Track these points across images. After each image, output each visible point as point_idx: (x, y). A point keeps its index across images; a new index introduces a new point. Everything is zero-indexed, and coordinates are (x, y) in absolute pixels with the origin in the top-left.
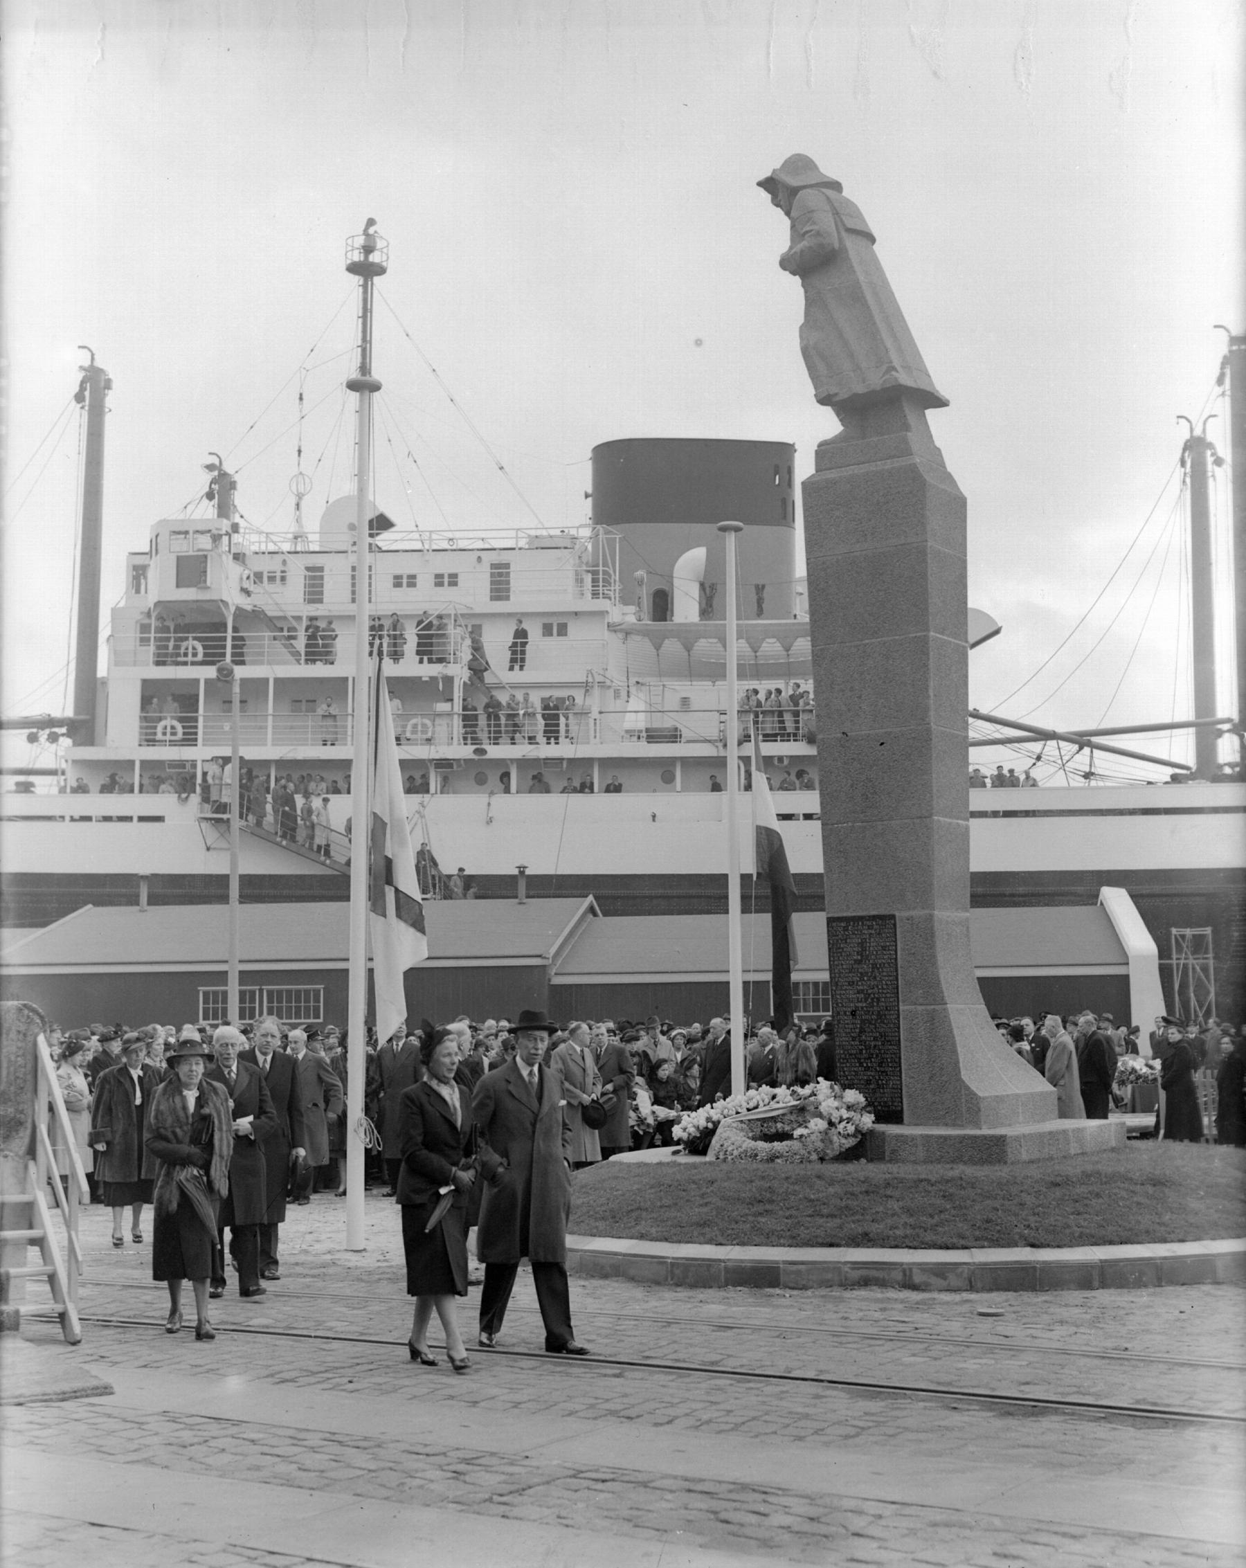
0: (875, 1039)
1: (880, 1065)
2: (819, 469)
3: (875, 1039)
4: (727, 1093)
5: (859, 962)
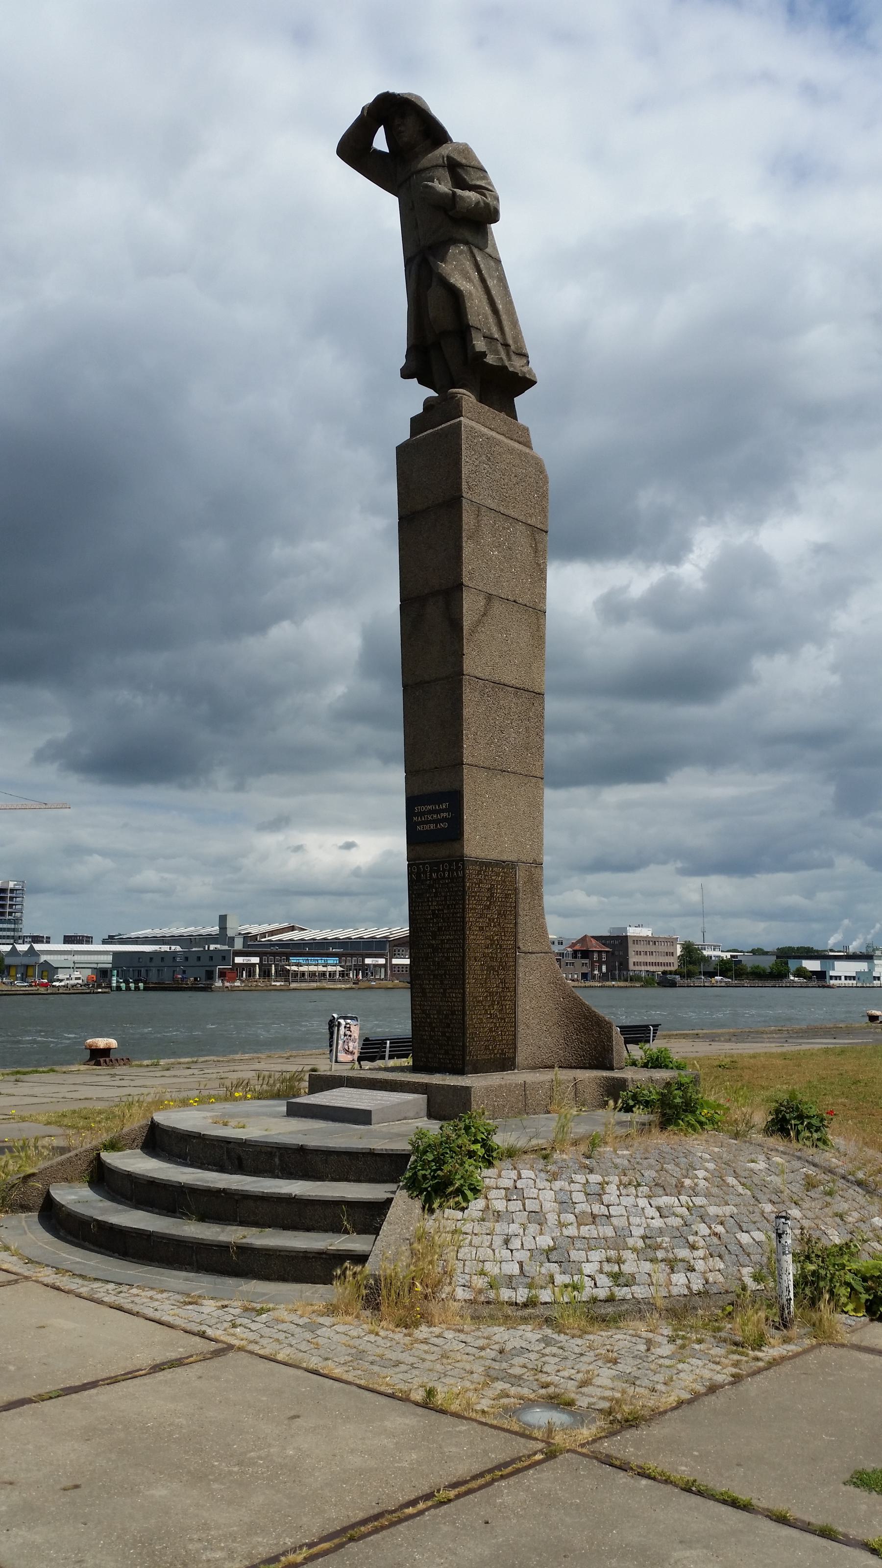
2: (413, 433)
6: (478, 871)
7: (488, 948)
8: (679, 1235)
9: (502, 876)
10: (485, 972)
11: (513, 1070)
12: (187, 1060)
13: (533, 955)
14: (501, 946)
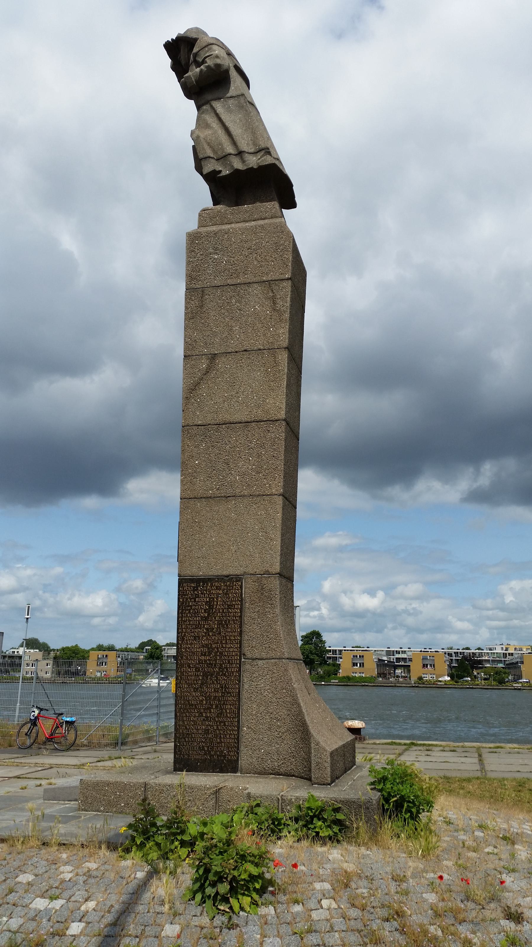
0: (216, 691)
1: (219, 715)
2: (201, 225)
3: (216, 691)
4: (213, 888)
5: (206, 619)
6: (194, 587)
7: (205, 655)
8: (20, 930)
10: (201, 678)
12: (492, 745)
14: (221, 653)
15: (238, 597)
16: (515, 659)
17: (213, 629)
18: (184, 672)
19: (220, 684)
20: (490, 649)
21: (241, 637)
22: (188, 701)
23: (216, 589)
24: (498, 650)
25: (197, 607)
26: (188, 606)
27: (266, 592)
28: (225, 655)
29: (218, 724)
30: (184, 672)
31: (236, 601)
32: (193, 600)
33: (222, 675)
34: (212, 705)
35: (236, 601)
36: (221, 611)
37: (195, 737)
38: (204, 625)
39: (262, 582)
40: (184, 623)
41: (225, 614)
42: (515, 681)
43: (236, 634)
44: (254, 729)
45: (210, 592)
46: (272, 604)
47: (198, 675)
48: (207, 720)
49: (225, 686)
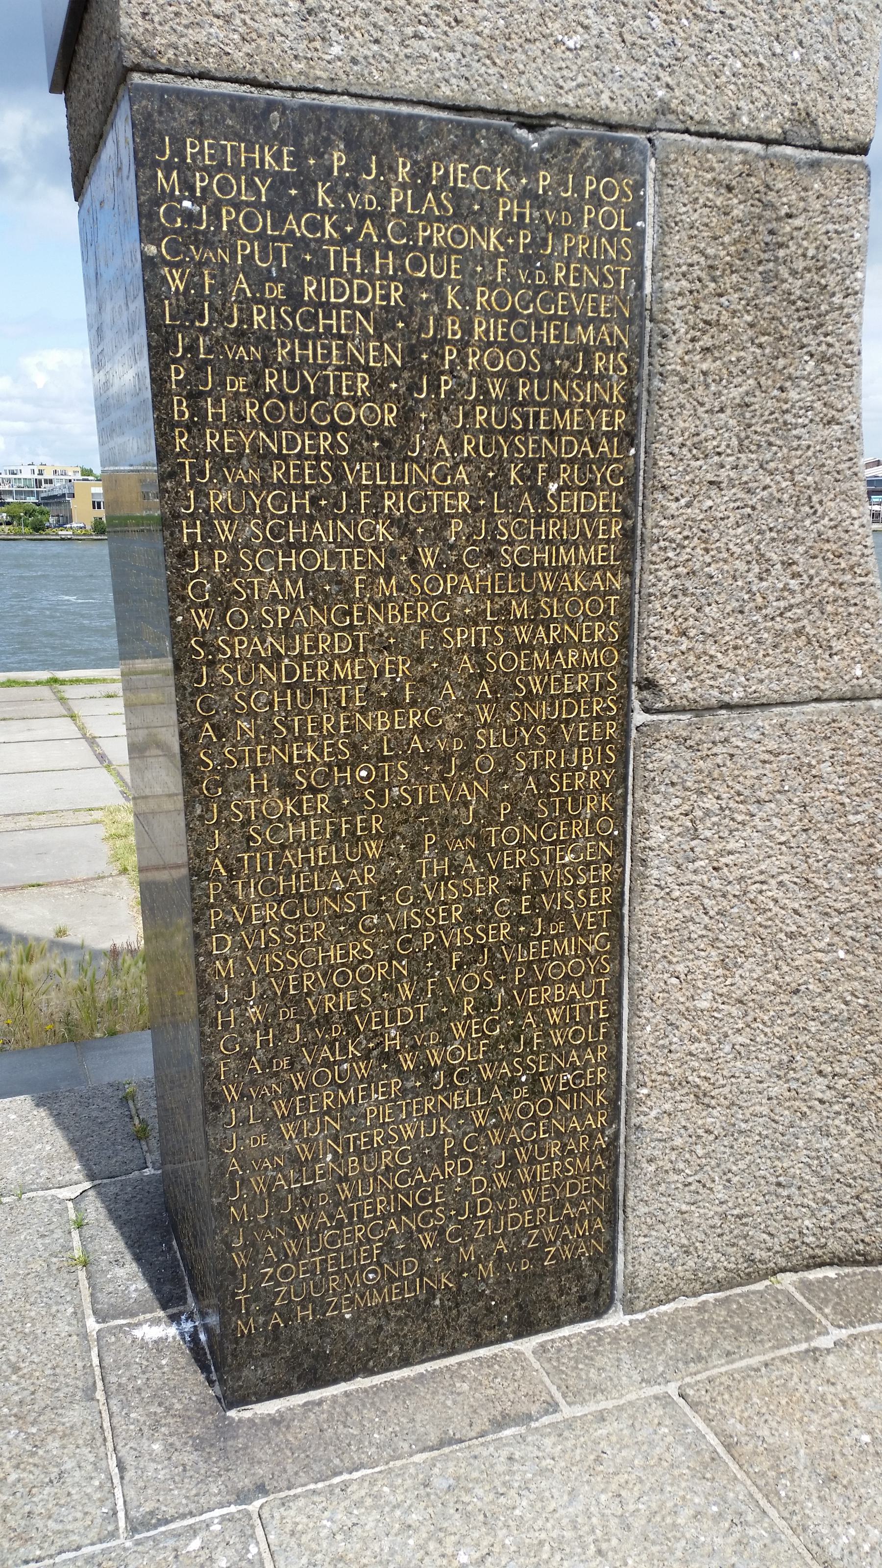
6: (280, 181)
7: (393, 703)
9: (512, 227)
10: (373, 850)
11: (598, 1314)
13: (759, 718)
15: (616, 290)
16: (58, 487)
17: (444, 521)
18: (247, 823)
19: (499, 871)
20: (13, 473)
21: (630, 573)
22: (298, 1001)
23: (457, 216)
24: (26, 474)
25: (313, 352)
26: (240, 336)
27: (794, 273)
28: (530, 697)
29: (497, 1094)
30: (247, 823)
31: (598, 322)
32: (279, 291)
33: (510, 819)
34: (455, 1001)
35: (598, 322)
36: (496, 391)
37: (355, 1198)
38: (376, 493)
39: (772, 196)
40: (216, 470)
41: (525, 417)
42: (61, 525)
43: (594, 555)
44: (705, 1086)
45: (409, 231)
46: (825, 359)
47: (352, 832)
48: (429, 1088)
49: (536, 879)
